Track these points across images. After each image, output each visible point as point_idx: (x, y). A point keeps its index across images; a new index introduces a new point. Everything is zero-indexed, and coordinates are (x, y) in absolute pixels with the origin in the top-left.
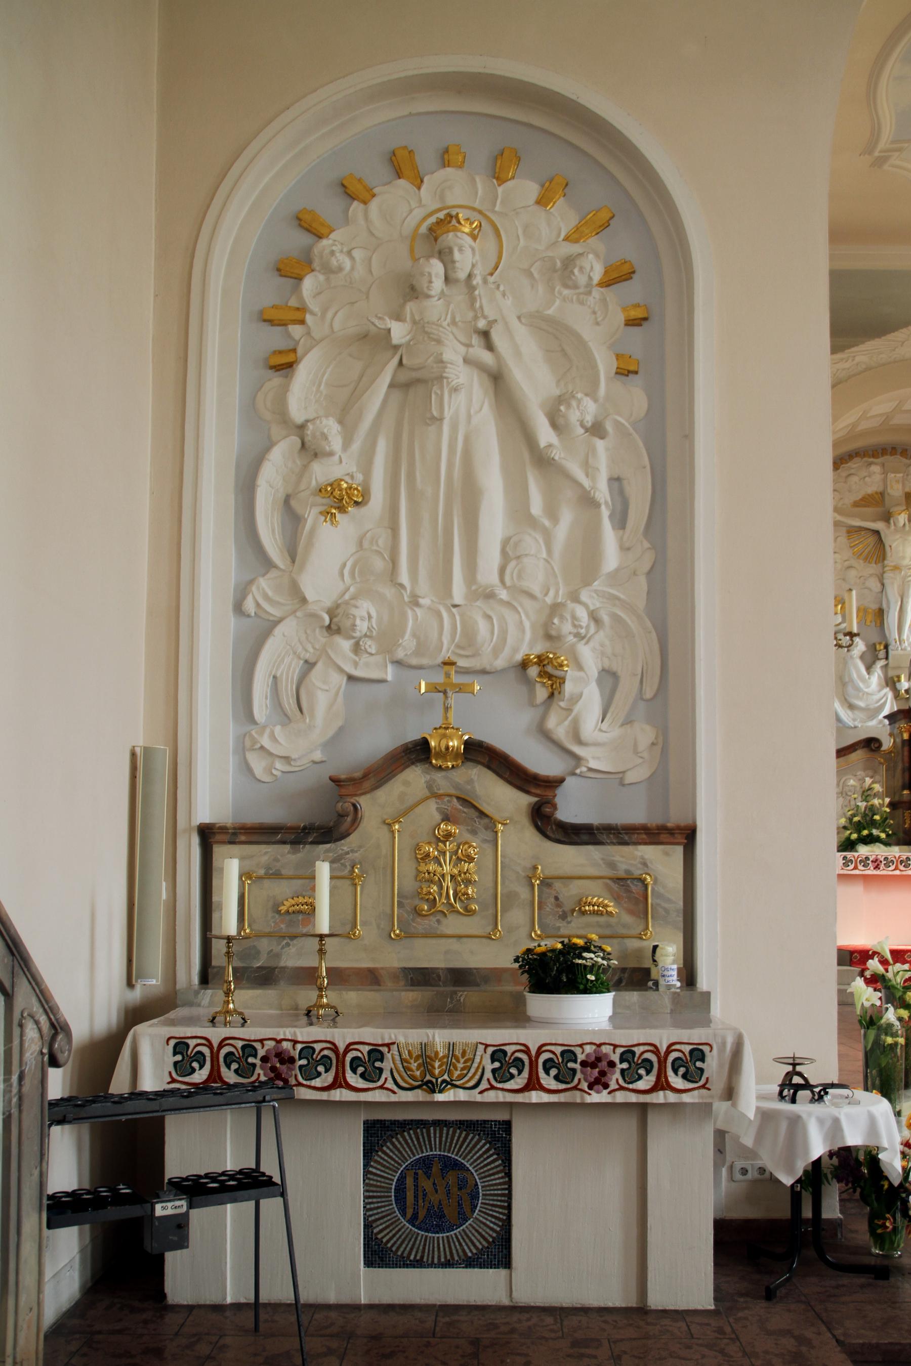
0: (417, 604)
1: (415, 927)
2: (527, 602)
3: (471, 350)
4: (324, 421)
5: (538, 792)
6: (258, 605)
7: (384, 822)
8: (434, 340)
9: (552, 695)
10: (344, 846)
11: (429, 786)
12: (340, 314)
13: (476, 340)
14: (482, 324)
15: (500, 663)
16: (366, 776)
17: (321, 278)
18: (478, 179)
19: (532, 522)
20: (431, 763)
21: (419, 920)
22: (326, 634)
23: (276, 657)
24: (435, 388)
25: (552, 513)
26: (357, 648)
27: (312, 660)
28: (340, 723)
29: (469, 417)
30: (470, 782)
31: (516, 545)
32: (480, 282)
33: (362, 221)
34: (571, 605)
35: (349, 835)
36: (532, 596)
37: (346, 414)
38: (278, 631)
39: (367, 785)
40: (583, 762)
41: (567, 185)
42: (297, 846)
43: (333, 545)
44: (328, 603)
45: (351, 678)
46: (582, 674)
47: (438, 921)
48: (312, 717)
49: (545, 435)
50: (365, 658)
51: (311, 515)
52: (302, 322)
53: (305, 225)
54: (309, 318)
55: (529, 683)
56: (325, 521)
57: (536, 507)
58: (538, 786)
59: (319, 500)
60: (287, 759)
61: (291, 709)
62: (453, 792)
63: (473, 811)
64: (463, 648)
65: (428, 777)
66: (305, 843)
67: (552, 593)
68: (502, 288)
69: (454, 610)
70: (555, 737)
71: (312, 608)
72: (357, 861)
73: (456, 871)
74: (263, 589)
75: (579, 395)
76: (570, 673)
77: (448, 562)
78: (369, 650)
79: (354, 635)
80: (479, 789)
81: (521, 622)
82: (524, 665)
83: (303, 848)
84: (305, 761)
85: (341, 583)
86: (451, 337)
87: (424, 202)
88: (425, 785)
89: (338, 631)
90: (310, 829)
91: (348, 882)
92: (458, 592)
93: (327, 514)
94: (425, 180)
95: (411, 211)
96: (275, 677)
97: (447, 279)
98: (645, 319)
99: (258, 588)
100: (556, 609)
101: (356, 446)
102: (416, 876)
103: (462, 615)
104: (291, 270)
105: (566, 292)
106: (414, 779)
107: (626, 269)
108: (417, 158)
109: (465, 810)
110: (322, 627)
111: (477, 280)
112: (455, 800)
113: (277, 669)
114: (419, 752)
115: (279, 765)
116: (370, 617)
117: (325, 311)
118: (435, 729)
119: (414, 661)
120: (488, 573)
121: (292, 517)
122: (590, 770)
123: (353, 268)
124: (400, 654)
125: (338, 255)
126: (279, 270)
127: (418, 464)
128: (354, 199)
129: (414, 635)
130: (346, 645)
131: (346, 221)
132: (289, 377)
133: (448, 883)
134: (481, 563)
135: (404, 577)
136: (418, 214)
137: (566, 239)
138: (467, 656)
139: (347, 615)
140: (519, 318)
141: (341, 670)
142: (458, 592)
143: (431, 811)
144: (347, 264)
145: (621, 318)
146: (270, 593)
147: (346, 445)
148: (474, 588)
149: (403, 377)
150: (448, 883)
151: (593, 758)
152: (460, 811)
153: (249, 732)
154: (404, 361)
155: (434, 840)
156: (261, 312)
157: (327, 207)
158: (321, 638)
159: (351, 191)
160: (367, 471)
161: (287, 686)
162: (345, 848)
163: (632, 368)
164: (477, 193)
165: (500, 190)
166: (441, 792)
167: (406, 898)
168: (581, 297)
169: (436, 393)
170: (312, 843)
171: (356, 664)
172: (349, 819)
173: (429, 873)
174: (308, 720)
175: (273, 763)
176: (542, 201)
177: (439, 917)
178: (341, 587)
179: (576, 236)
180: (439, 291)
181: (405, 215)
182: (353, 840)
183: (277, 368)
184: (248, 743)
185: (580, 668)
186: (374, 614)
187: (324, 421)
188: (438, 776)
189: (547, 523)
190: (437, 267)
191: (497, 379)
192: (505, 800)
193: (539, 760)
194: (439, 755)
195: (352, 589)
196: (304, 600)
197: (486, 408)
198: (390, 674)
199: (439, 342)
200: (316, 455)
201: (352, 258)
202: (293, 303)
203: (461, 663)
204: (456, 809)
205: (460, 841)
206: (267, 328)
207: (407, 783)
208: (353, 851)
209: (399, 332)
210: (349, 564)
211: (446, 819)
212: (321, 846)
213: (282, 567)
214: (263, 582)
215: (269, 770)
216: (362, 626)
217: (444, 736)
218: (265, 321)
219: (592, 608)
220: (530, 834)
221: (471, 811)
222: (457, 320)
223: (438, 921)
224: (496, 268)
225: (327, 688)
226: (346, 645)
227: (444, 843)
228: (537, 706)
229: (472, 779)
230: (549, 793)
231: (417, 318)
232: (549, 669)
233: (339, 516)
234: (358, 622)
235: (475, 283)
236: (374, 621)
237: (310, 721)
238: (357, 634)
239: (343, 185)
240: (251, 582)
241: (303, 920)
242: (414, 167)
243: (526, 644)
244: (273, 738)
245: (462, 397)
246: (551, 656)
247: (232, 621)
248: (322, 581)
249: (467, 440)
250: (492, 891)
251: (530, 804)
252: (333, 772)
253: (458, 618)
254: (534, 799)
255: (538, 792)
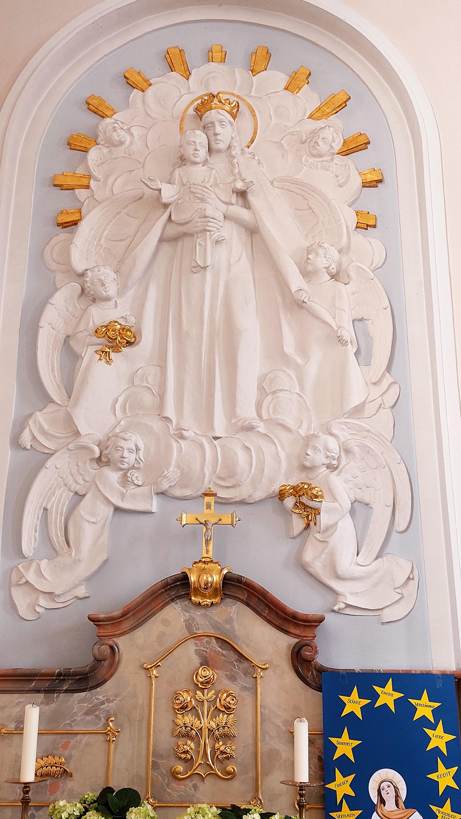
0: (182, 437)
1: (169, 794)
2: (283, 434)
3: (231, 207)
4: (102, 269)
5: (297, 632)
6: (34, 438)
7: (142, 667)
8: (199, 199)
9: (308, 526)
10: (100, 694)
11: (189, 627)
12: (119, 181)
13: (234, 199)
14: (240, 185)
15: (259, 495)
16: (124, 615)
17: (105, 150)
18: (237, 71)
19: (285, 359)
20: (190, 599)
21: (174, 785)
22: (96, 466)
23: (48, 491)
24: (198, 241)
25: (303, 350)
26: (125, 481)
27: (82, 492)
28: (105, 557)
29: (229, 266)
30: (229, 621)
31: (271, 381)
32: (239, 152)
33: (140, 105)
34: (324, 437)
35: (105, 681)
36: (287, 429)
37: (121, 263)
38: (50, 463)
39: (126, 625)
40: (341, 598)
41: (310, 74)
42: (51, 695)
43: (106, 379)
44: (100, 436)
45: (117, 509)
46: (336, 505)
47: (195, 786)
48: (78, 551)
49: (296, 281)
50: (132, 490)
51: (89, 354)
52: (87, 187)
53: (93, 108)
54: (93, 184)
55: (286, 513)
56: (100, 359)
57: (289, 347)
58: (297, 625)
59: (95, 339)
60: (50, 595)
61: (59, 543)
62: (211, 631)
63: (232, 653)
64: (220, 478)
65: (188, 615)
66: (59, 692)
67: (305, 425)
68: (257, 158)
69: (215, 442)
70: (311, 570)
71: (84, 441)
72: (112, 712)
73: (213, 725)
74: (39, 423)
75: (326, 245)
76: (325, 505)
77: (211, 396)
78: (136, 482)
79: (122, 466)
80: (239, 630)
81: (277, 453)
82: (281, 495)
83: (57, 697)
84: (69, 597)
85: (113, 417)
86: (214, 196)
87: (191, 90)
88: (184, 624)
89: (108, 463)
90: (65, 675)
91: (101, 738)
92: (220, 426)
93: (104, 354)
94: (193, 72)
95: (181, 97)
96: (45, 509)
97: (210, 150)
98: (380, 181)
99: (35, 422)
100: (308, 440)
101: (131, 293)
102: (173, 731)
103: (222, 447)
104: (78, 145)
105: (312, 160)
106: (174, 616)
107: (362, 140)
108: (187, 57)
109: (224, 652)
110: (92, 460)
111: (236, 151)
112: (214, 641)
113: (48, 502)
114: (179, 587)
115: (43, 602)
116: (138, 449)
117: (107, 177)
118: (195, 563)
119: (178, 492)
120: (247, 410)
121: (70, 354)
122: (348, 606)
123: (131, 143)
124: (165, 486)
125: (118, 131)
126: (69, 144)
127: (184, 308)
128: (134, 88)
129: (178, 466)
130: (114, 476)
131: (127, 105)
132: (73, 233)
133: (206, 740)
134: (240, 397)
135: (170, 412)
136: (187, 99)
137: (310, 117)
138: (227, 487)
139: (117, 448)
140: (272, 183)
141: (109, 502)
142: (220, 426)
143: (189, 654)
144: (128, 139)
145: (358, 181)
146: (46, 427)
147: (121, 292)
148: (233, 421)
149: (172, 231)
150: (206, 740)
151: (351, 594)
152: (218, 653)
153: (16, 567)
154: (173, 218)
155: (192, 687)
156: (54, 178)
157: (111, 94)
158: (91, 469)
159: (133, 82)
160: (140, 316)
161: (56, 518)
162: (100, 697)
163: (371, 223)
164: (236, 81)
165: (255, 79)
166: (200, 632)
167: (161, 757)
168: (325, 163)
169: (200, 244)
170: (67, 691)
171: (123, 496)
172: (106, 663)
173: (186, 727)
174: (73, 553)
175: (37, 598)
176: (292, 87)
177: (196, 780)
178: (113, 421)
179: (318, 114)
180: (203, 159)
181: (176, 100)
182: (109, 687)
183: (64, 225)
184: (14, 579)
185: (335, 499)
186: (141, 446)
187: (102, 269)
188: (198, 614)
189: (299, 361)
190: (200, 138)
191: (253, 231)
192: (266, 642)
193: (298, 598)
194: (197, 591)
195: (122, 423)
196: (77, 434)
197: (244, 259)
198: (154, 505)
199: (203, 200)
200: (94, 300)
201: (132, 135)
202: (80, 171)
203: (222, 494)
204: (215, 651)
205: (218, 688)
206: (57, 191)
207: (166, 622)
208: (108, 701)
209: (168, 193)
210: (121, 400)
211: (205, 662)
212: (76, 695)
213: (59, 402)
214: (39, 416)
215: (33, 607)
216: (130, 458)
217: (203, 570)
218: (55, 185)
219: (343, 439)
220: (291, 678)
221: (229, 652)
222: (219, 182)
223: (195, 786)
224: (252, 141)
225: (94, 520)
226: (114, 476)
227: (202, 690)
228: (294, 538)
229: (231, 618)
230: (308, 633)
231: (185, 181)
232: (304, 500)
233: (113, 355)
234: (126, 454)
235: (234, 153)
236: (141, 453)
237: (76, 555)
238: (126, 466)
239: (125, 77)
240: (30, 415)
241: (51, 784)
242: (184, 63)
243: (284, 476)
244: (39, 573)
245: (222, 250)
246: (306, 487)
247: (8, 454)
248: (95, 416)
249: (227, 287)
250: (251, 749)
251: (290, 645)
252: (93, 612)
253: (219, 449)
254: (295, 641)
255: (297, 632)
